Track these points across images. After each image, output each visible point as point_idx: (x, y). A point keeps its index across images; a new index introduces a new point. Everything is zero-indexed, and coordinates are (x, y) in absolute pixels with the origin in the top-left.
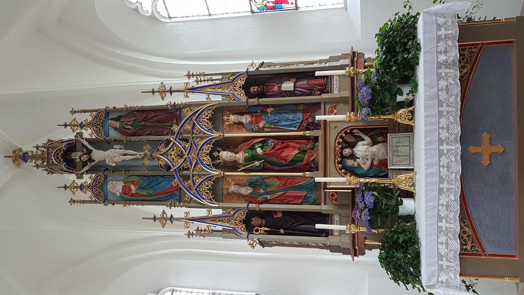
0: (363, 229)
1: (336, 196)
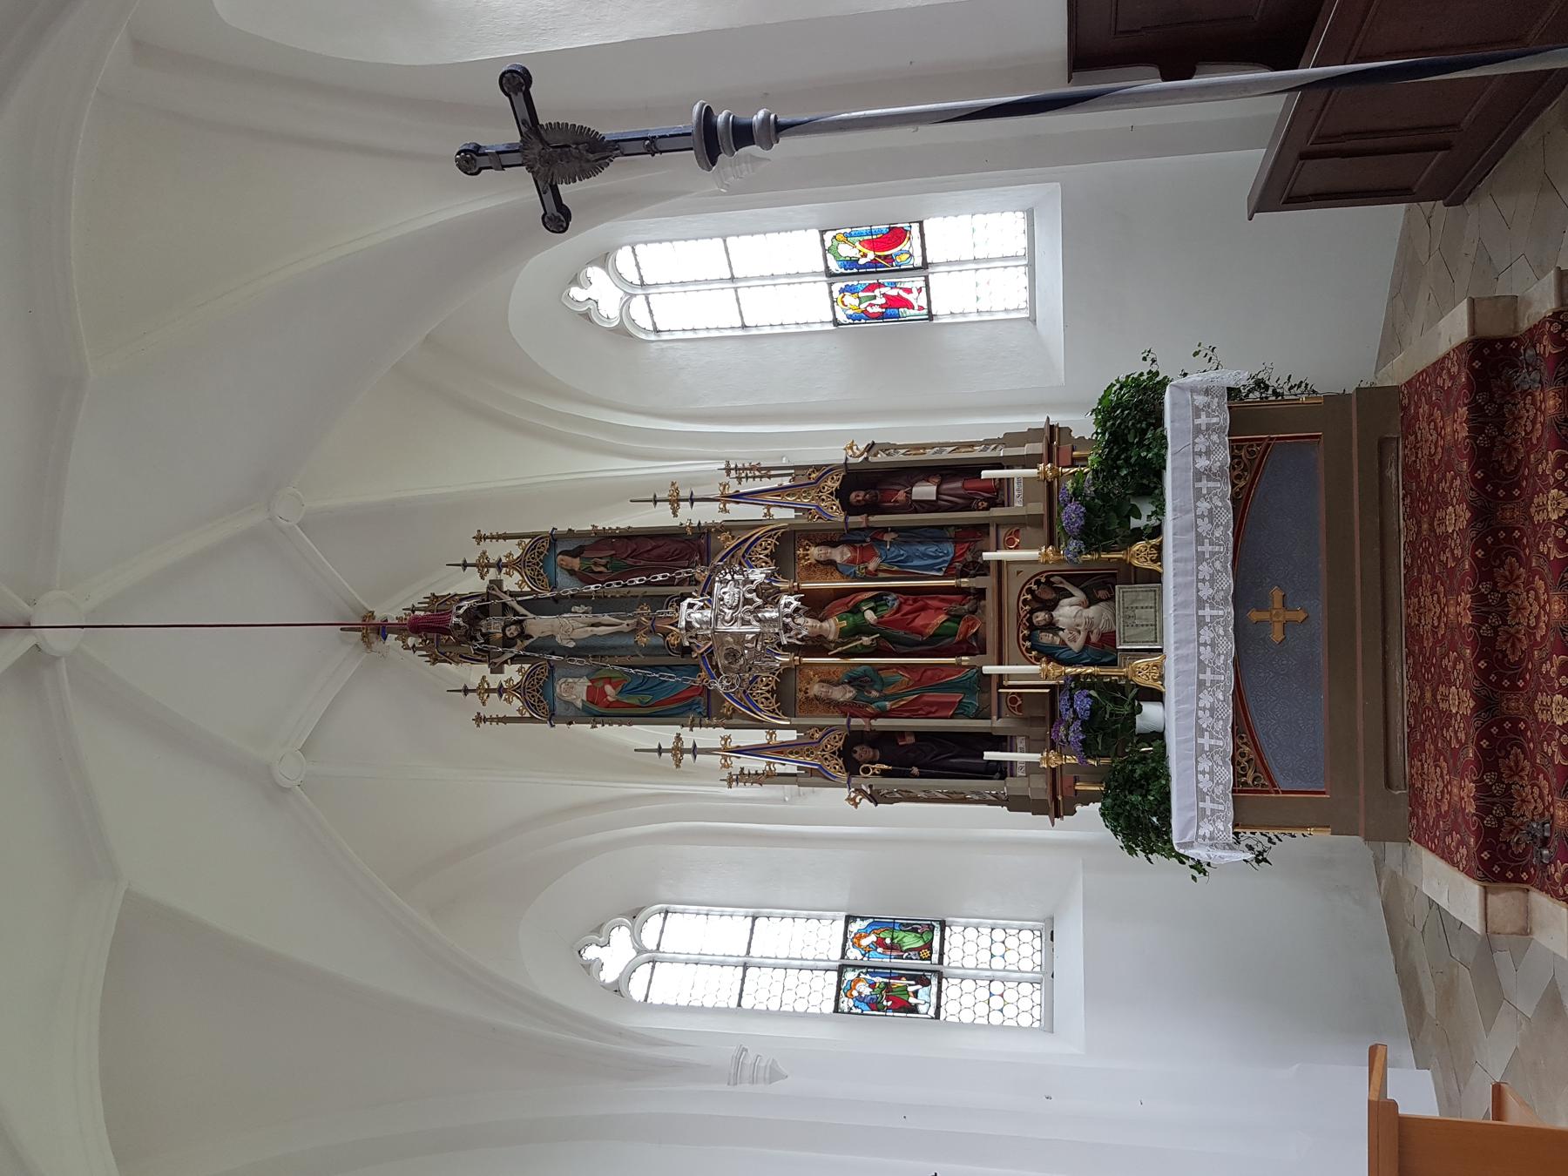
0: (1071, 760)
1: (1020, 702)
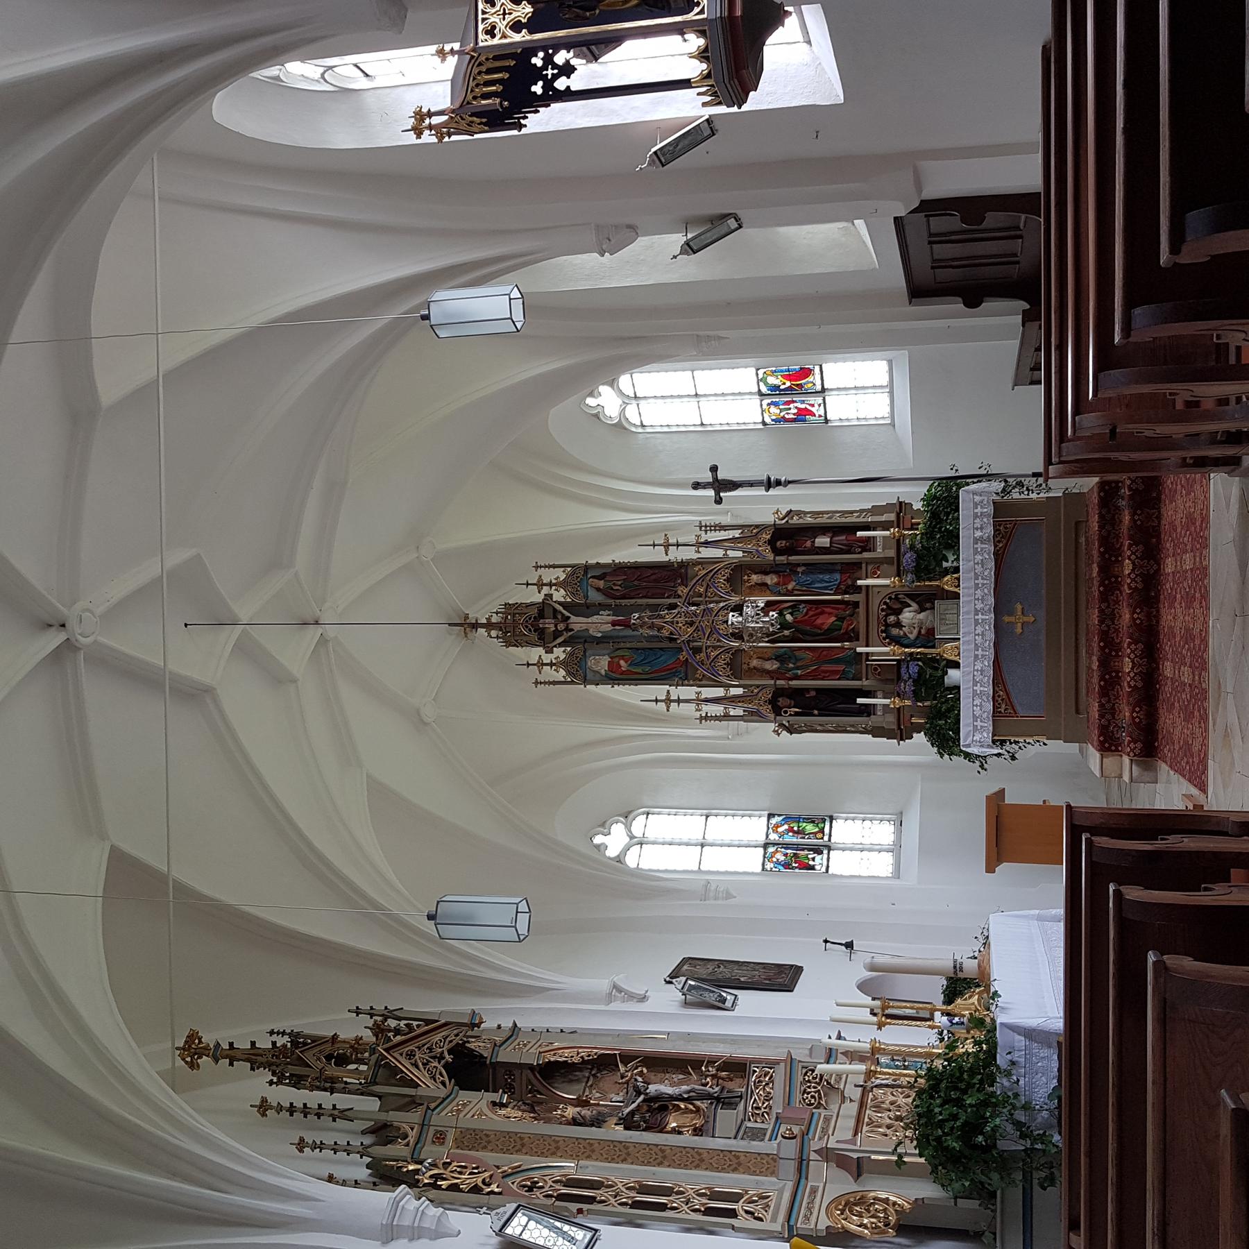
0: (908, 703)
